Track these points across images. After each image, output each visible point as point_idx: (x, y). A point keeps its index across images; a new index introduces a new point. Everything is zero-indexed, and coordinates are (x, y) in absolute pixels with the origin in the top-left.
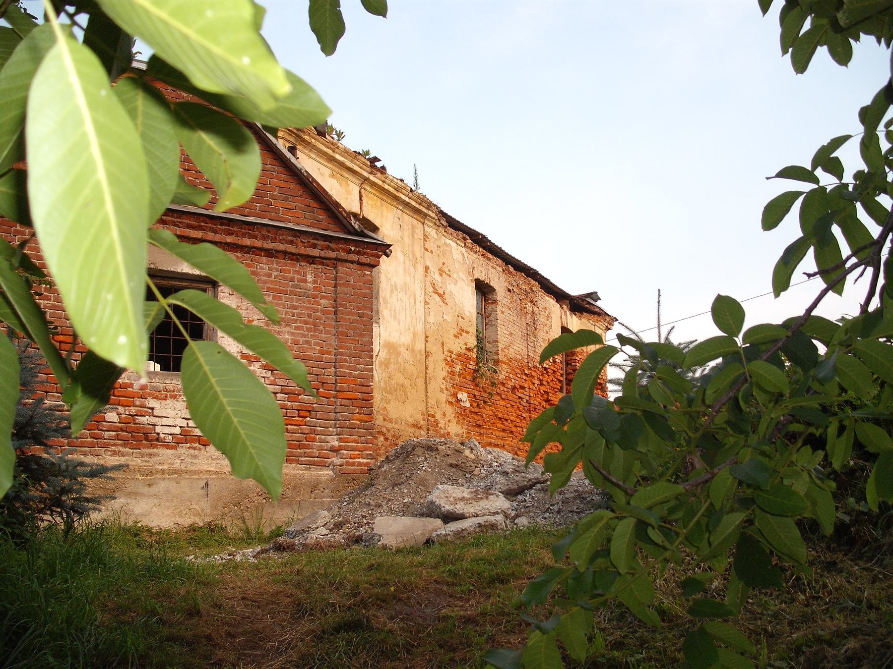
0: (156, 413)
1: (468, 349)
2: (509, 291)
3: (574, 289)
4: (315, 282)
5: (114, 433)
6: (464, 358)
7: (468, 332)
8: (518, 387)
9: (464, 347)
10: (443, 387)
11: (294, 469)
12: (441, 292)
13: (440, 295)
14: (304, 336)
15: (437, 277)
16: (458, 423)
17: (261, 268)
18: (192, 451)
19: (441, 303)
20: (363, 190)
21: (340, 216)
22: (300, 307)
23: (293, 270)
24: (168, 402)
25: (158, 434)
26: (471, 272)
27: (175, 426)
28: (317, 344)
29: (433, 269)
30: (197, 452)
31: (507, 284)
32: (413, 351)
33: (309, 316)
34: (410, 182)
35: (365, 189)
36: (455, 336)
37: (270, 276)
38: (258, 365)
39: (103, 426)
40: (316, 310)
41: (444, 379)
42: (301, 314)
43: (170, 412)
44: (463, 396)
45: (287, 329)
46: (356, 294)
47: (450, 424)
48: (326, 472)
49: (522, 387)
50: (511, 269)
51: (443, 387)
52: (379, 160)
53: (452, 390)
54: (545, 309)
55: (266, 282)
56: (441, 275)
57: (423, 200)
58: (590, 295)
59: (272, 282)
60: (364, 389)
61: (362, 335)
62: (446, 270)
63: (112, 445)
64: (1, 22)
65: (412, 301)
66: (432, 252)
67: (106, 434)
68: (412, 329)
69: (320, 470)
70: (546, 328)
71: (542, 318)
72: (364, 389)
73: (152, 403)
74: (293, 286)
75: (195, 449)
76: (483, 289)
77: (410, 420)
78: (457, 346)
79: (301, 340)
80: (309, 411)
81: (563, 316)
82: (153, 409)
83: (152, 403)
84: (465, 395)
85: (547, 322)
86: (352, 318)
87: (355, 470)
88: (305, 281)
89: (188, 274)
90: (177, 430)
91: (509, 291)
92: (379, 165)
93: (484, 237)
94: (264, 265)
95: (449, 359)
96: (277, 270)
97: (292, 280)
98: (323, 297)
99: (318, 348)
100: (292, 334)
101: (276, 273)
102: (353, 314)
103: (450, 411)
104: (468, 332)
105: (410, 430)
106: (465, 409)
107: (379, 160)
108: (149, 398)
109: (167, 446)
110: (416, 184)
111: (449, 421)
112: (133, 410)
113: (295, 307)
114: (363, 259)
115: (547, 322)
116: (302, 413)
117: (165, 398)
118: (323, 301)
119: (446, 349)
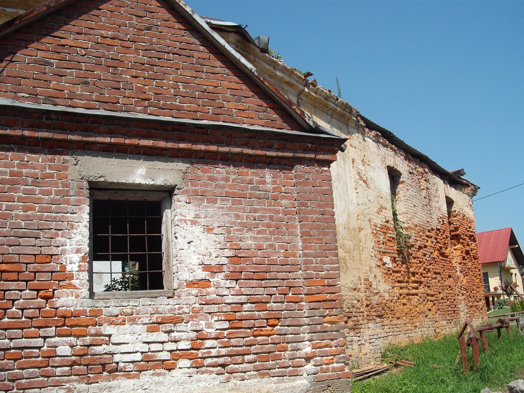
0: (114, 339)
1: (387, 222)
2: (410, 173)
3: (450, 169)
4: (274, 182)
5: (67, 369)
6: (384, 229)
7: (386, 209)
8: (423, 246)
9: (384, 220)
10: (373, 255)
11: (267, 383)
12: (364, 178)
13: (365, 182)
14: (267, 240)
15: (361, 167)
16: (385, 282)
17: (218, 172)
18: (156, 378)
19: (366, 188)
20: (300, 100)
21: (295, 115)
22: (262, 209)
23: (250, 174)
24: (127, 326)
25: (117, 363)
26: (383, 161)
27: (136, 352)
28: (281, 247)
29: (358, 160)
30: (161, 378)
31: (408, 168)
32: (349, 229)
33: (271, 218)
34: (335, 93)
35: (302, 99)
36: (378, 213)
37: (227, 180)
38: (221, 276)
39: (54, 362)
40: (278, 212)
41: (373, 248)
42: (262, 217)
43: (127, 338)
44: (387, 259)
45: (250, 234)
46: (316, 191)
47: (380, 284)
48: (302, 381)
49: (426, 247)
50: (410, 157)
51: (373, 255)
52: (312, 75)
53: (379, 256)
54: (434, 184)
55: (223, 187)
56: (364, 165)
57: (347, 107)
58: (458, 171)
59: (230, 186)
60: (331, 289)
61: (326, 234)
62: (366, 161)
63: (67, 382)
64: (521, 384)
65: (345, 189)
66: (355, 147)
67: (58, 371)
68: (346, 210)
69: (294, 380)
70: (436, 199)
71: (432, 191)
72: (331, 289)
73: (107, 329)
74: (253, 189)
75: (159, 375)
76: (394, 176)
77: (351, 286)
78: (379, 221)
79: (265, 245)
80: (278, 319)
81: (446, 189)
82: (110, 336)
83: (107, 329)
84: (389, 258)
85: (436, 194)
86: (315, 216)
87: (329, 376)
88: (264, 182)
89: (140, 185)
90: (138, 357)
91: (410, 173)
92: (310, 79)
93: (390, 133)
94: (220, 171)
95: (375, 231)
96: (234, 173)
97: (251, 182)
98: (284, 198)
99: (282, 251)
100: (255, 238)
101: (233, 177)
102: (314, 212)
103: (379, 272)
104: (386, 209)
105: (351, 294)
106: (389, 269)
107: (312, 75)
108: (105, 325)
109: (128, 375)
110: (340, 94)
111: (379, 281)
112: (88, 340)
113: (256, 211)
114: (321, 157)
115: (436, 194)
116: (271, 322)
117: (123, 323)
118: (284, 202)
119: (372, 224)
